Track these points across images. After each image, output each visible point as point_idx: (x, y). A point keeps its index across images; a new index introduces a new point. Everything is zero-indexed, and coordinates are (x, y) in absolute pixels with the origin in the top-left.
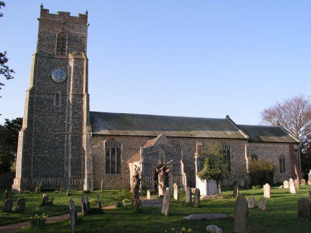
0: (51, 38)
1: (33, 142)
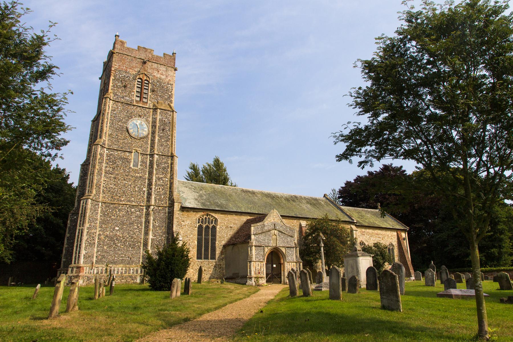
0: (129, 79)
1: (99, 214)
